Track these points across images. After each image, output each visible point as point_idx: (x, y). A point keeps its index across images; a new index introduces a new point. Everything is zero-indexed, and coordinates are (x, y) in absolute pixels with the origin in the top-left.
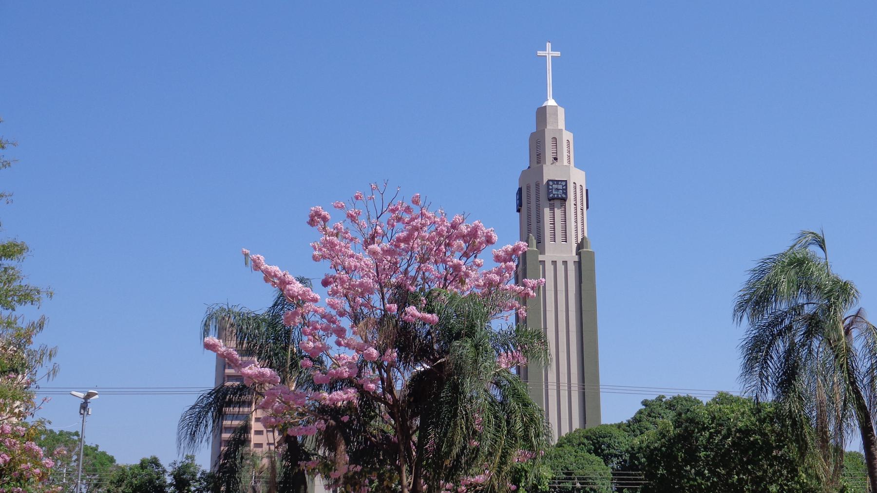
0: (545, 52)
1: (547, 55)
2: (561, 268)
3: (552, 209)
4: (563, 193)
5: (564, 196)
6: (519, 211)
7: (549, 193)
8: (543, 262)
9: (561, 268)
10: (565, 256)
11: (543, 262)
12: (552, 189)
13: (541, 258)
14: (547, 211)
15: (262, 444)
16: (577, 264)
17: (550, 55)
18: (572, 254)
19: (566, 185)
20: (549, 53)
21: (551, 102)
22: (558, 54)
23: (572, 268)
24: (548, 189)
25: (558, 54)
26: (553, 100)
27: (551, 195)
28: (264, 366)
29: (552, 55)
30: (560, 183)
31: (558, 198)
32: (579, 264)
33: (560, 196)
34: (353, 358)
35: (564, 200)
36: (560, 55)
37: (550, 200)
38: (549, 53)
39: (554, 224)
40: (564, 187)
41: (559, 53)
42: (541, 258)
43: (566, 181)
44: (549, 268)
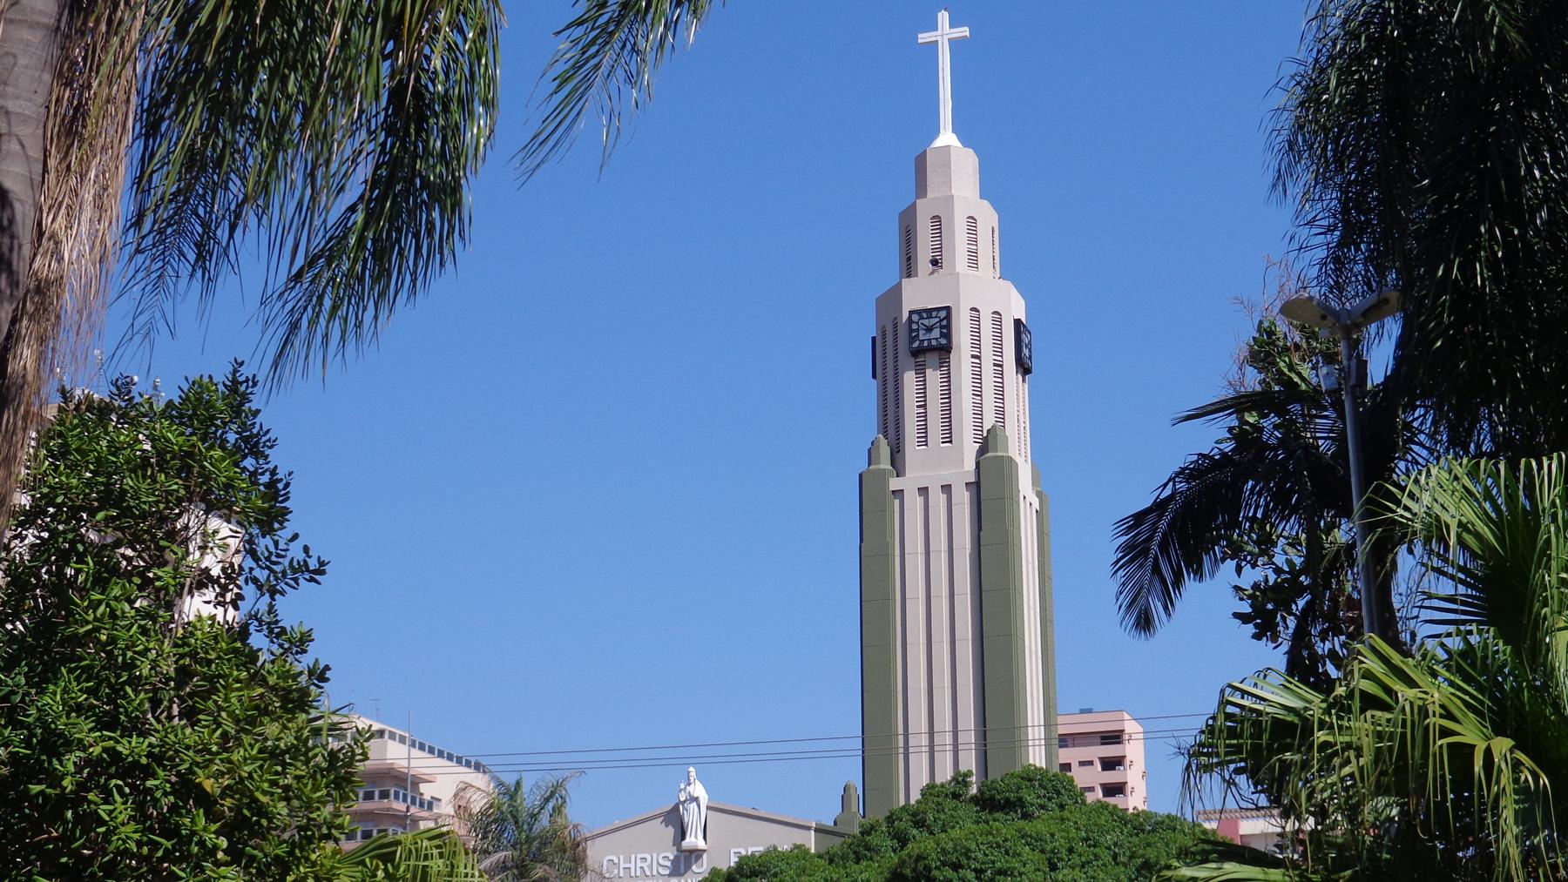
0: (934, 33)
1: (939, 39)
2: (938, 500)
3: (921, 370)
4: (942, 335)
5: (943, 341)
6: (874, 376)
7: (912, 340)
8: (899, 494)
9: (938, 500)
10: (946, 476)
11: (899, 494)
12: (918, 330)
13: (895, 484)
14: (910, 379)
15: (1069, 765)
16: (975, 486)
17: (946, 38)
18: (963, 467)
19: (948, 317)
20: (945, 32)
21: (947, 138)
22: (964, 31)
23: (963, 499)
24: (911, 331)
25: (964, 31)
26: (954, 136)
27: (916, 345)
28: (1465, 535)
29: (949, 36)
30: (934, 314)
31: (931, 349)
32: (976, 487)
33: (934, 343)
34: (1266, 580)
35: (944, 350)
36: (920, 36)
37: (915, 353)
38: (945, 32)
39: (924, 406)
40: (944, 323)
41: (967, 29)
42: (895, 484)
43: (948, 309)
44: (914, 503)
